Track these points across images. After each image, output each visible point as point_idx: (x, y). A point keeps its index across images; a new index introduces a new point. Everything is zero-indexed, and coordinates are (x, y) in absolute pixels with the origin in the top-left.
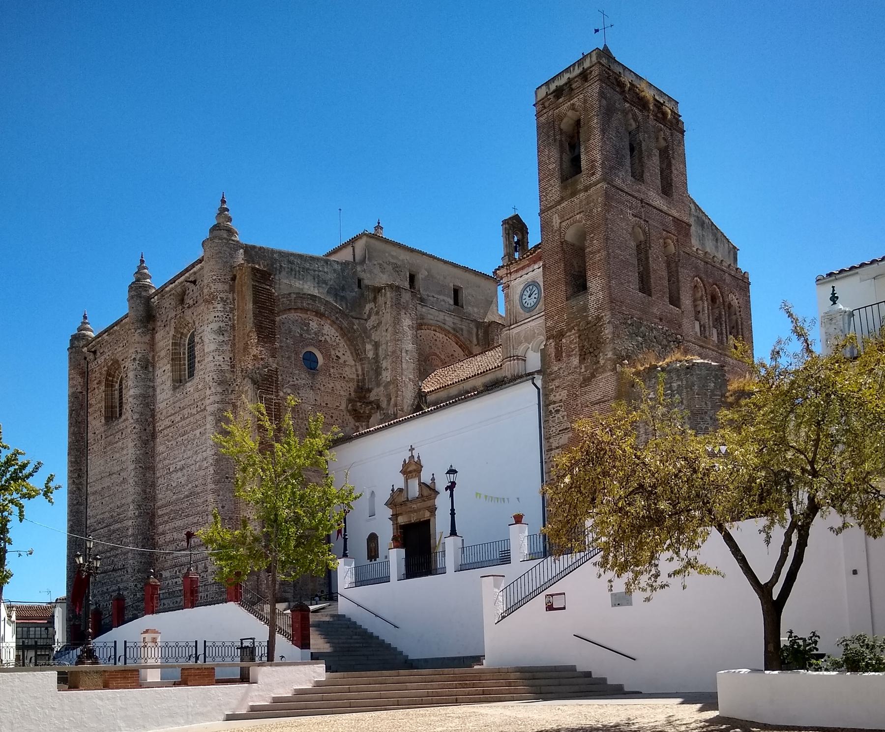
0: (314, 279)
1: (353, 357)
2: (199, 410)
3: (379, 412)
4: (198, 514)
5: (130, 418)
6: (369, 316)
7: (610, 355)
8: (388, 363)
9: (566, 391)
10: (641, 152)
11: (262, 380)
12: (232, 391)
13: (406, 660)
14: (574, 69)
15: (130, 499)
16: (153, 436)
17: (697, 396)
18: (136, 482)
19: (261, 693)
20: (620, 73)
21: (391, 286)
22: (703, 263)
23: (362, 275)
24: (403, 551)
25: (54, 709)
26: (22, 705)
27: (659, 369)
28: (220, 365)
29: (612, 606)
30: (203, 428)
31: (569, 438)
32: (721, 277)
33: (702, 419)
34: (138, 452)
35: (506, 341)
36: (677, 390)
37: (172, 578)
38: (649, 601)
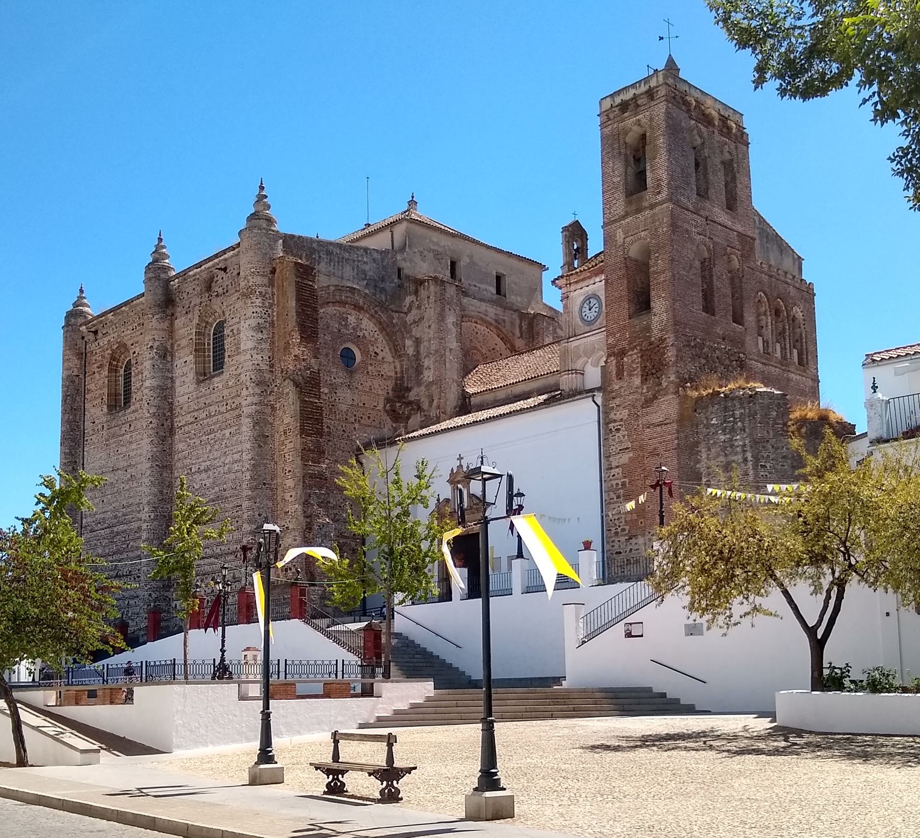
0: (353, 269)
1: (392, 353)
2: (229, 408)
3: (419, 413)
6: (410, 310)
7: (673, 378)
8: (431, 362)
9: (627, 411)
10: (706, 168)
11: (305, 383)
13: (470, 681)
14: (640, 86)
15: (145, 501)
16: (172, 431)
17: (759, 425)
18: (151, 482)
19: (384, 706)
20: (686, 91)
21: (435, 279)
22: (767, 277)
23: (402, 264)
24: (466, 570)
25: (235, 716)
26: (214, 711)
27: (722, 395)
28: (258, 364)
29: (686, 635)
31: (630, 458)
32: (786, 290)
33: (764, 447)
34: (155, 449)
35: (565, 353)
36: (739, 418)
38: (726, 635)
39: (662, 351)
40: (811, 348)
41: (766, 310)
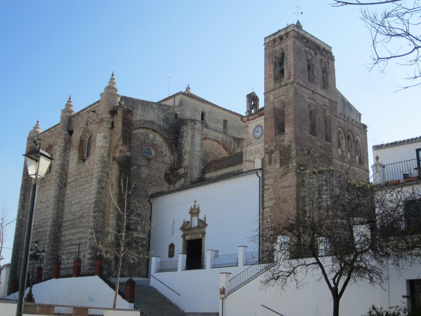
2: (90, 174)
4: (84, 227)
5: (54, 175)
7: (294, 164)
12: (108, 167)
15: (49, 217)
16: (65, 185)
30: (91, 184)
31: (273, 203)
37: (67, 259)
39: (289, 151)
40: (365, 156)
41: (343, 136)
